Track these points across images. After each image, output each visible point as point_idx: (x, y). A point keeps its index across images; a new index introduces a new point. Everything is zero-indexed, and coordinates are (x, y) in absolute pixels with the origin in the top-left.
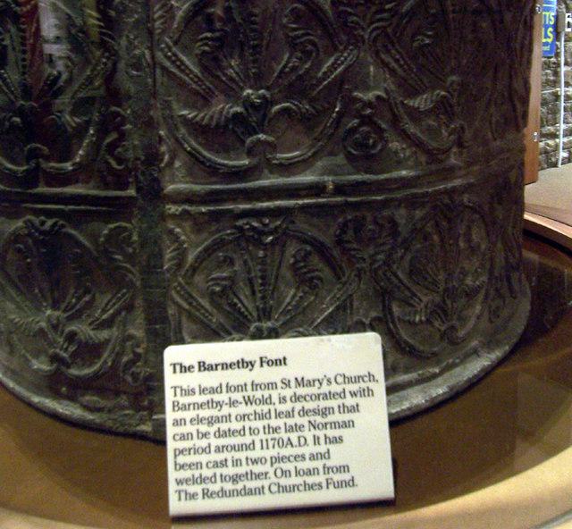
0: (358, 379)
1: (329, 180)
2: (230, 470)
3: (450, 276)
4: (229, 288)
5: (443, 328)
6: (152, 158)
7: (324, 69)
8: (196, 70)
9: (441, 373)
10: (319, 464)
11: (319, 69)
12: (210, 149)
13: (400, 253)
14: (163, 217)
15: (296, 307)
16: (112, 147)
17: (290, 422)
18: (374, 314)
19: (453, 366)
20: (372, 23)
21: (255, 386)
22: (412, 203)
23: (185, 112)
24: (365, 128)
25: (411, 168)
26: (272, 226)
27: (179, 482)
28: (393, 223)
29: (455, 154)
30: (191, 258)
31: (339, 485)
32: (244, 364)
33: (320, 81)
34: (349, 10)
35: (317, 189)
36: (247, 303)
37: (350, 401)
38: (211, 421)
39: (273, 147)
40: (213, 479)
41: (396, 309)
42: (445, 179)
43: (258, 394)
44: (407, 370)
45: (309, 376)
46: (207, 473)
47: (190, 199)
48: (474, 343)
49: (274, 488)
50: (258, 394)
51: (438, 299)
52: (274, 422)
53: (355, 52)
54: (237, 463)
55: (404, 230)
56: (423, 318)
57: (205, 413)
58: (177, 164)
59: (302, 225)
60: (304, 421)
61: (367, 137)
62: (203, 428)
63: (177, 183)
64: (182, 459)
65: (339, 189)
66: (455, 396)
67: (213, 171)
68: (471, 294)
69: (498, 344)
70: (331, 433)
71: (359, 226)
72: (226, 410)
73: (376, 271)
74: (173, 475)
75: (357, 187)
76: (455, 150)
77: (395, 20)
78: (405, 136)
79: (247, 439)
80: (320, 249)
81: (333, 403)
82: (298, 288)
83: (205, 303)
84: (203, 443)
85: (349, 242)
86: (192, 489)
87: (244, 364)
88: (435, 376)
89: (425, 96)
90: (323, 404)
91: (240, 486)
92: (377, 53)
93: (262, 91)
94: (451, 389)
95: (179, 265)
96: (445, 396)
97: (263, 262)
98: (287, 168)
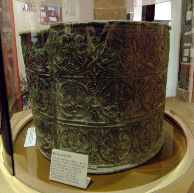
0: (83, 164)
1: (87, 122)
2: (59, 174)
3: (116, 146)
4: (68, 139)
5: (115, 157)
6: (55, 112)
7: (86, 100)
8: (63, 97)
9: (113, 166)
10: (74, 178)
11: (85, 99)
12: (65, 112)
13: (102, 139)
14: (57, 123)
15: (80, 146)
16: (50, 108)
17: (70, 168)
18: (96, 150)
19: (117, 166)
20: (96, 91)
21: (65, 160)
22: (105, 129)
23: (61, 104)
24: (94, 113)
25: (105, 121)
26: (75, 129)
27: (51, 174)
28: (101, 133)
29: (118, 119)
30: (62, 131)
31: (76, 183)
32: (65, 156)
33: (86, 101)
34: (91, 89)
35: (84, 123)
36: (71, 143)
37: (81, 168)
38: (58, 165)
39: (77, 113)
40: (56, 175)
41: (102, 150)
42: (116, 125)
43: (66, 162)
44: (104, 164)
45: (75, 161)
46: (56, 174)
47: (61, 121)
48: (126, 162)
49: (66, 180)
50: (66, 162)
51: (113, 150)
52: (68, 168)
53: (92, 97)
54: (61, 173)
55: (103, 135)
56: (108, 154)
57: (57, 163)
58: (60, 114)
59: (81, 130)
60: (72, 169)
61: (94, 114)
62: (56, 165)
63: (59, 117)
64: (52, 170)
65: (89, 124)
66: (115, 172)
67: (65, 116)
68: (124, 151)
69: (134, 163)
70: (77, 173)
71: (93, 132)
72: (60, 163)
73: (96, 142)
74: (51, 172)
75: (92, 124)
76: (118, 118)
77: (101, 91)
78: (103, 115)
79: (63, 169)
80: (84, 135)
81: (78, 167)
82: (80, 142)
83: (64, 141)
84: (56, 168)
85: (91, 135)
86: (53, 176)
87: (65, 156)
88: (111, 167)
89: (109, 107)
90: (76, 167)
91: (60, 178)
92: (97, 97)
93: (74, 103)
94: (115, 171)
95: (59, 133)
96: (112, 172)
97: (74, 135)
98: (79, 118)
